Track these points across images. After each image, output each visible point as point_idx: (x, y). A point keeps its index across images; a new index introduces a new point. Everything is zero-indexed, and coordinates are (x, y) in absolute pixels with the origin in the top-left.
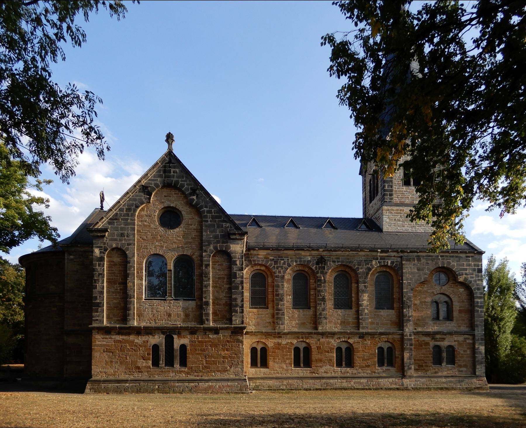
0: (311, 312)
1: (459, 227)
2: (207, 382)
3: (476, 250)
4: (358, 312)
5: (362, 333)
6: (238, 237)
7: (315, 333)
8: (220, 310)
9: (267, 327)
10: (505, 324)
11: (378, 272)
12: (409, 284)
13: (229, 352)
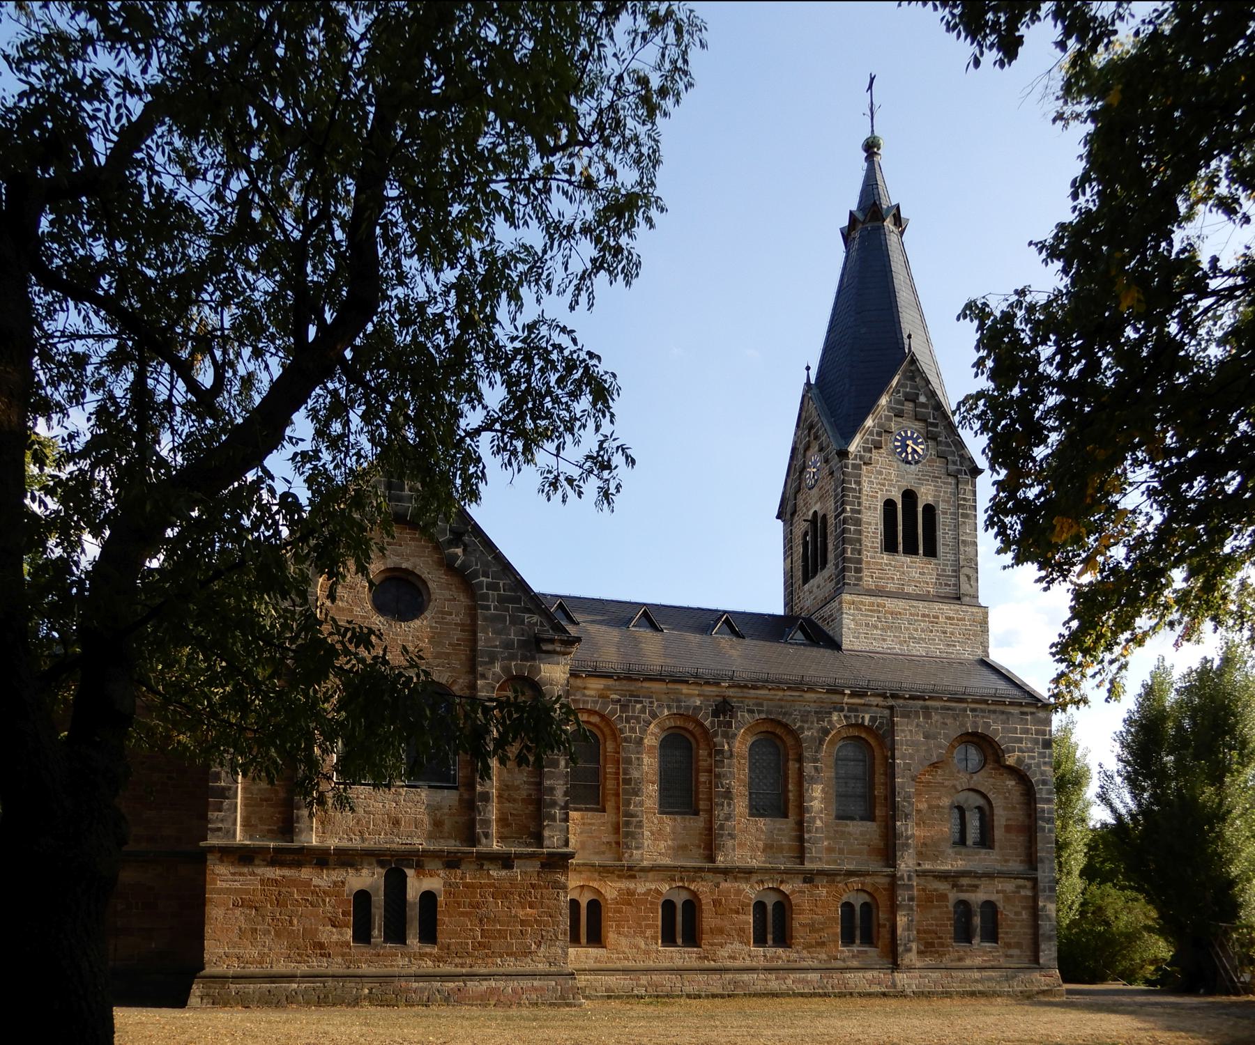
0: (699, 822)
1: (1120, 668)
2: (486, 980)
3: (1039, 700)
4: (800, 824)
5: (811, 872)
6: (558, 649)
7: (710, 870)
8: (514, 812)
9: (604, 853)
10: (1069, 855)
11: (844, 738)
12: (908, 767)
13: (534, 911)
